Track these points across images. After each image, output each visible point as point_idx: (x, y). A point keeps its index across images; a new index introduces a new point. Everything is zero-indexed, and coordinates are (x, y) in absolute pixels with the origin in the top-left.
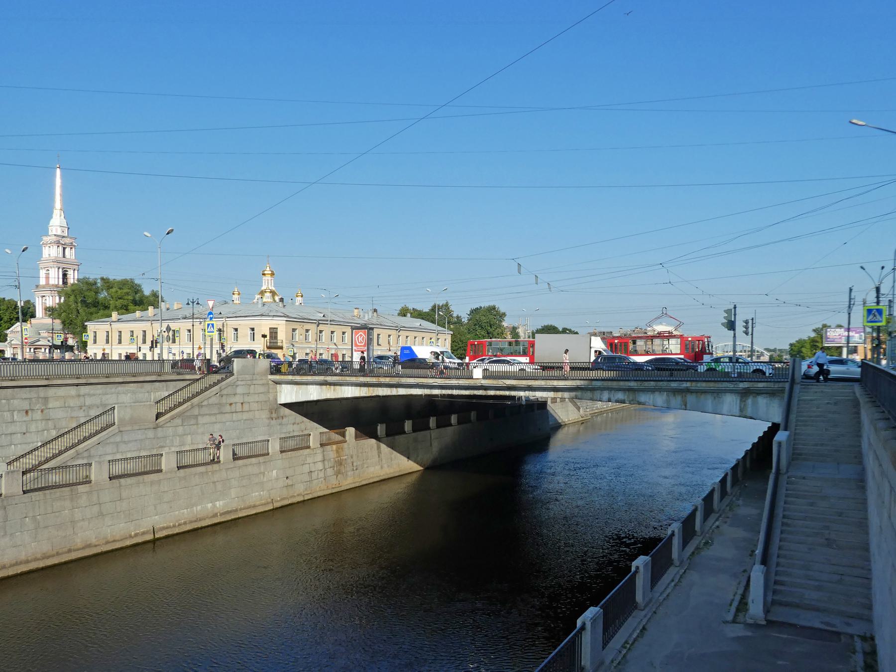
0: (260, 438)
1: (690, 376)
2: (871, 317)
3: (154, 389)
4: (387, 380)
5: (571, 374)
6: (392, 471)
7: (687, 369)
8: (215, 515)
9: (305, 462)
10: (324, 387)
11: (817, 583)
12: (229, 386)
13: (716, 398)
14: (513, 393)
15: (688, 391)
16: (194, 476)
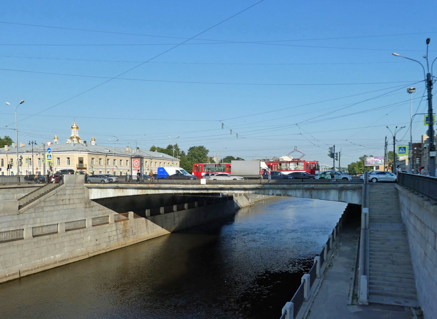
0: (80, 219)
1: (280, 182)
2: (401, 151)
3: (16, 192)
4: (153, 186)
5: (234, 181)
6: (154, 234)
7: (310, 178)
8: (56, 262)
9: (106, 231)
10: (117, 190)
11: (389, 283)
12: (61, 190)
13: (327, 192)
14: (219, 192)
15: (313, 189)
16: (43, 241)
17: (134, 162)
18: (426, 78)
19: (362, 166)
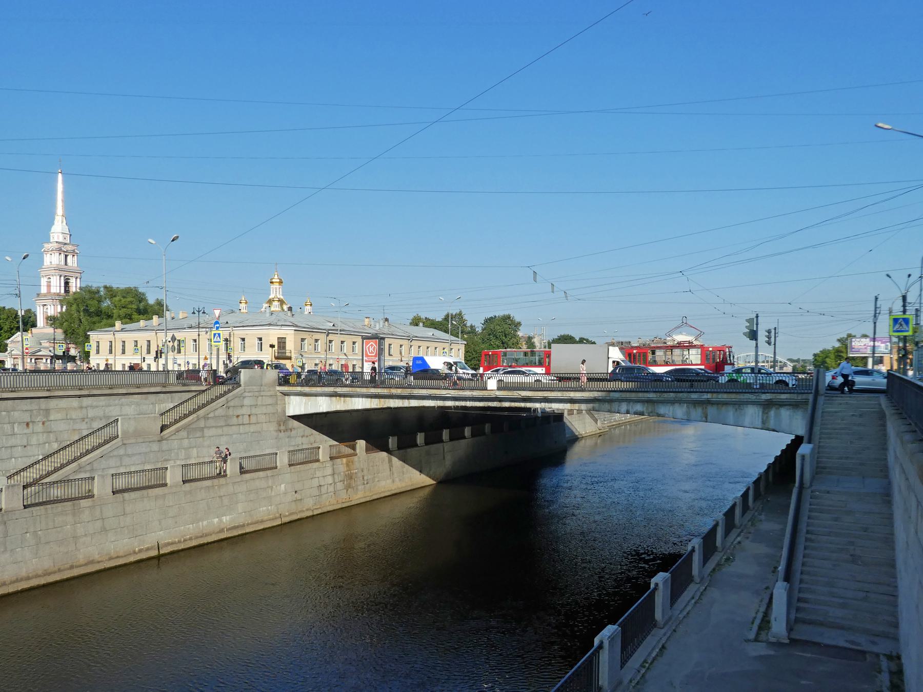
0: (267, 452)
1: (711, 387)
2: (897, 326)
3: (159, 400)
4: (399, 391)
5: (588, 385)
6: (404, 485)
7: (708, 380)
8: (222, 531)
9: (315, 476)
10: (334, 399)
11: (841, 601)
12: (236, 397)
13: (738, 409)
14: (529, 405)
15: (709, 402)
16: (200, 491)
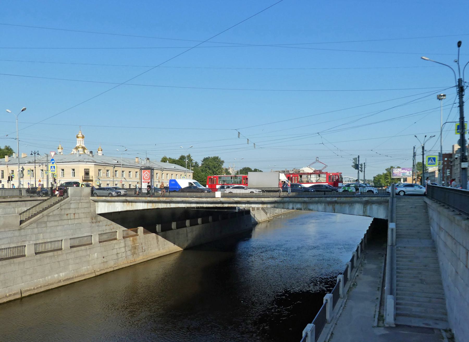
0: (85, 235)
1: (300, 195)
2: (430, 161)
3: (17, 206)
4: (164, 199)
5: (251, 194)
6: (165, 251)
7: (332, 191)
8: (60, 281)
9: (114, 248)
10: (125, 204)
11: (418, 303)
12: (66, 203)
13: (351, 206)
14: (235, 205)
15: (336, 202)
16: (46, 259)
17: (144, 174)
18: (457, 84)
19: (388, 178)
